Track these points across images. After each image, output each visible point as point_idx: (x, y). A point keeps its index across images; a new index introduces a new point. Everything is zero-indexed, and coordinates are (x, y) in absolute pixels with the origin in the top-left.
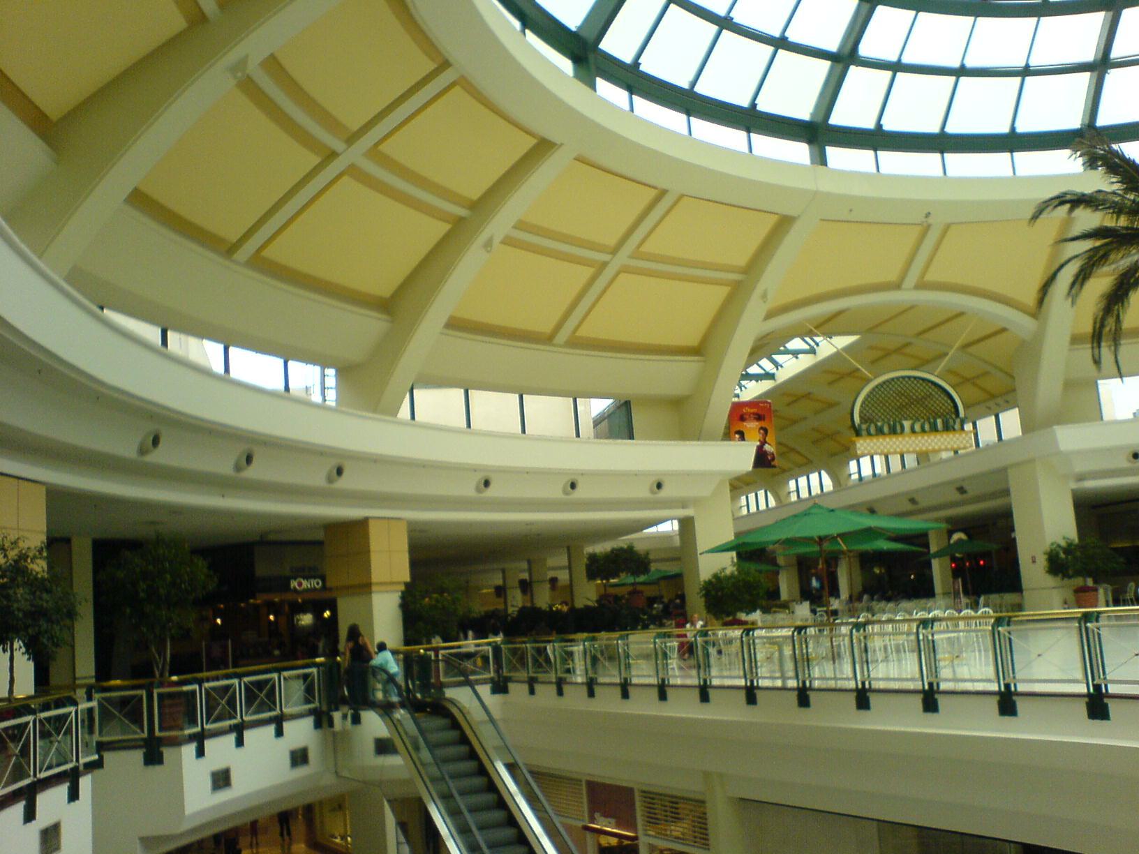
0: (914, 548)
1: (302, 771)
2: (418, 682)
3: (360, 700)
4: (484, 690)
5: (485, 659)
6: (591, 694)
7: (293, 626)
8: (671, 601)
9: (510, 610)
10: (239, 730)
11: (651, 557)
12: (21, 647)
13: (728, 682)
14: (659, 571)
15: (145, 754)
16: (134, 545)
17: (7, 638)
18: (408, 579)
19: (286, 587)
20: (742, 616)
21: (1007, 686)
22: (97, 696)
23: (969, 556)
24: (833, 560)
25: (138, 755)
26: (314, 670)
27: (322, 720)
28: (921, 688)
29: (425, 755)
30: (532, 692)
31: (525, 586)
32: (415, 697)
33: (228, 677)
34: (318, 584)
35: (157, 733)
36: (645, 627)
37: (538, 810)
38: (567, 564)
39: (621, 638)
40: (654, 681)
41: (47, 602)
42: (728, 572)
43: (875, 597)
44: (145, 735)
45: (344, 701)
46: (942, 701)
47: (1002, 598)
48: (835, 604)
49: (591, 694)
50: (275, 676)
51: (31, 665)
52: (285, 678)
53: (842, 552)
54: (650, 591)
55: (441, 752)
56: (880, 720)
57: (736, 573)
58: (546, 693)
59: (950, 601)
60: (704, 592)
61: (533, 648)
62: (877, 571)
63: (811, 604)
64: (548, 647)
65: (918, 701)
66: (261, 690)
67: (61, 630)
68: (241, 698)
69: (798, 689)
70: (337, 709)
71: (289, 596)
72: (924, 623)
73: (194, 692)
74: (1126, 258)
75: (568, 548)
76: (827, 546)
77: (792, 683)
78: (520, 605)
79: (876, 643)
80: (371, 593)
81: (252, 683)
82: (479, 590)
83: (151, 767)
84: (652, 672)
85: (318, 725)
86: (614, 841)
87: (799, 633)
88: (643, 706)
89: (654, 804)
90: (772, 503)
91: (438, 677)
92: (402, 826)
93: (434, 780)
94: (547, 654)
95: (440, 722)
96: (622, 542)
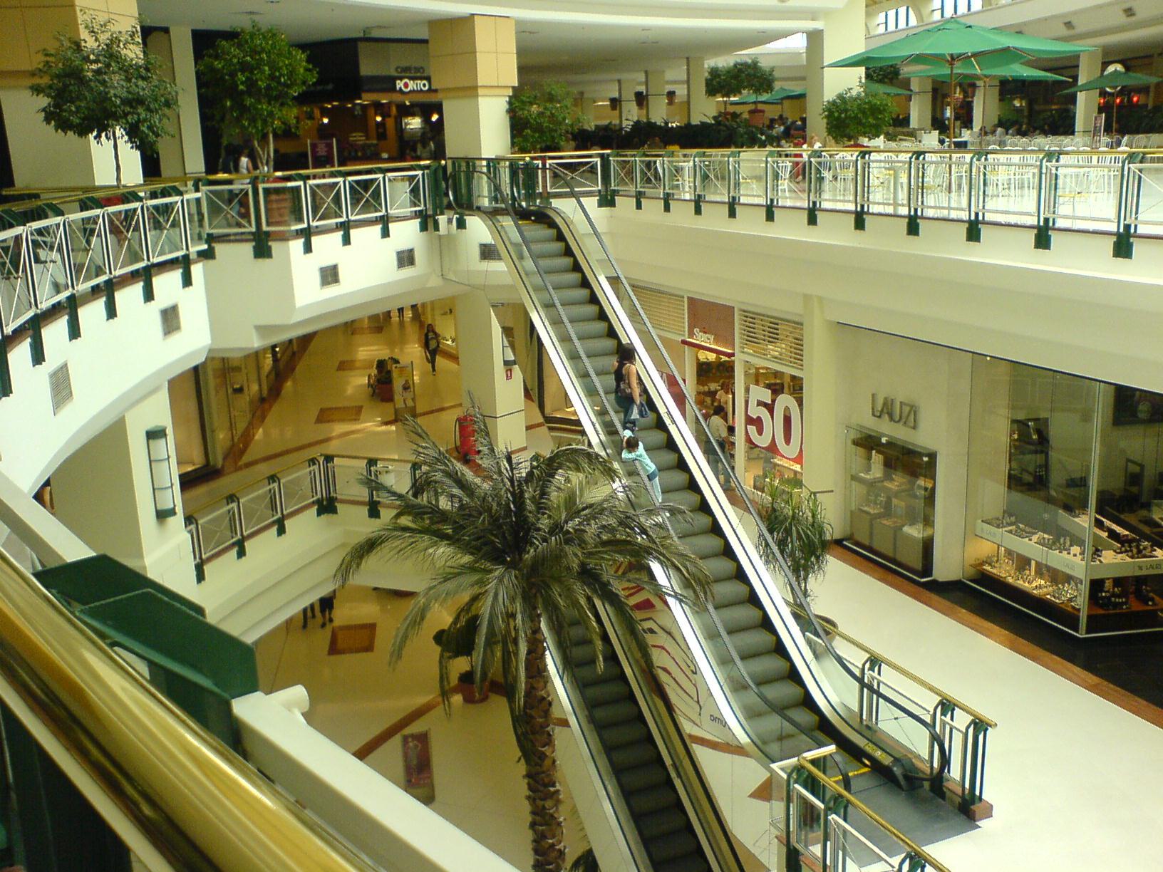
0: (1064, 78)
1: (408, 272)
2: (523, 192)
3: (465, 205)
4: (591, 203)
5: (593, 169)
6: (698, 211)
7: (400, 130)
8: (794, 123)
9: (625, 123)
10: (346, 227)
11: (776, 74)
12: (123, 136)
13: (839, 206)
14: (782, 89)
15: (254, 247)
16: (231, 35)
17: (108, 125)
19: (393, 89)
20: (865, 141)
21: (1127, 227)
22: (204, 188)
23: (1126, 91)
24: (969, 86)
25: (248, 248)
26: (419, 173)
27: (427, 222)
28: (1036, 223)
29: (529, 264)
30: (639, 206)
31: (641, 99)
32: (521, 206)
33: (333, 175)
34: (424, 85)
35: (265, 228)
36: (763, 145)
37: (635, 322)
38: (685, 78)
39: (733, 155)
40: (762, 201)
41: (144, 89)
42: (854, 93)
43: (1010, 131)
44: (253, 229)
45: (449, 207)
46: (1055, 237)
47: (1149, 138)
48: (966, 136)
49: (698, 211)
50: (380, 176)
51: (137, 154)
52: (390, 180)
53: (978, 77)
54: (772, 112)
55: (542, 262)
56: (992, 253)
57: (863, 94)
58: (652, 208)
59: (1088, 139)
60: (826, 113)
61: (642, 162)
62: (1017, 103)
63: (940, 133)
64: (658, 161)
65: (1031, 236)
66: (366, 191)
67: (160, 120)
68: (346, 198)
69: (910, 217)
70: (442, 213)
71: (397, 98)
72: (1050, 155)
73: (298, 188)
75: (688, 58)
76: (959, 69)
77: (904, 211)
78: (635, 119)
79: (1001, 176)
80: (477, 96)
81: (357, 182)
82: (595, 102)
83: (260, 260)
84: (762, 193)
85: (424, 228)
86: (712, 357)
87: (917, 158)
88: (750, 225)
89: (754, 324)
90: (913, 21)
91: (545, 187)
92: (507, 331)
93: (536, 289)
94: (656, 168)
95: (542, 231)
96: (745, 55)
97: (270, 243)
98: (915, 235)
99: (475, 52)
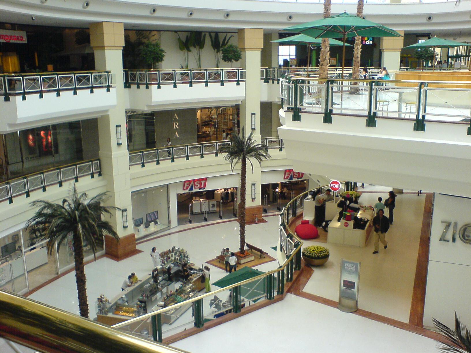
18: (124, 45)
74: (319, 38)
80: (104, 49)
83: (6, 102)
97: (9, 97)
98: (372, 126)
99: (103, 34)
